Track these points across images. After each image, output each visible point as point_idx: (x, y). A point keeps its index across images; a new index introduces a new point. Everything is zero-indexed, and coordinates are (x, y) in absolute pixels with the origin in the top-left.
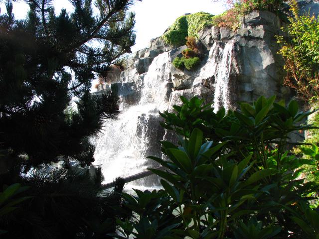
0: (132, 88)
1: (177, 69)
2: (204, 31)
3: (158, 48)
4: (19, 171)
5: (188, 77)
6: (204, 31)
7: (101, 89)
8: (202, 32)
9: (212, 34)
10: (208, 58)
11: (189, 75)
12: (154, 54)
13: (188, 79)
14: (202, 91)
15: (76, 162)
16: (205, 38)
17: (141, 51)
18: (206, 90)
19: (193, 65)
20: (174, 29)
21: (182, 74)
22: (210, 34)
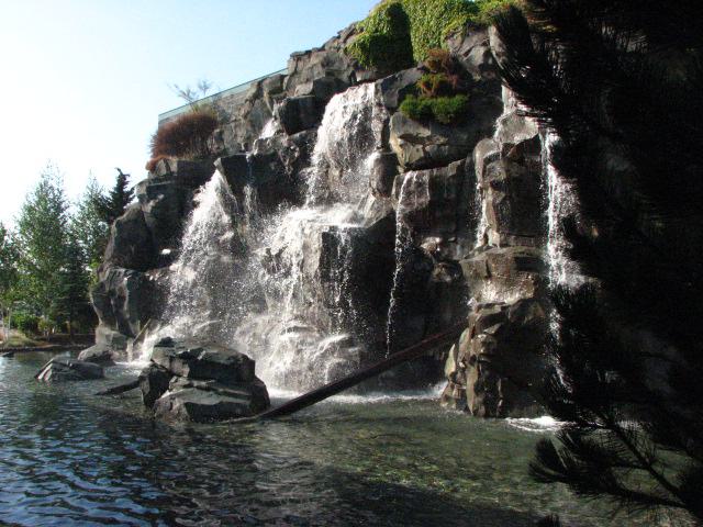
0: (272, 166)
1: (410, 122)
2: (465, 36)
3: (328, 74)
4: (603, 287)
5: (442, 140)
6: (465, 36)
7: (164, 172)
8: (458, 38)
9: (492, 44)
10: (518, 98)
11: (442, 135)
12: (331, 85)
13: (439, 146)
14: (507, 171)
15: (109, 373)
16: (469, 51)
17: (267, 81)
18: (516, 170)
19: (456, 113)
20: (377, 31)
21: (426, 133)
22: (486, 44)
